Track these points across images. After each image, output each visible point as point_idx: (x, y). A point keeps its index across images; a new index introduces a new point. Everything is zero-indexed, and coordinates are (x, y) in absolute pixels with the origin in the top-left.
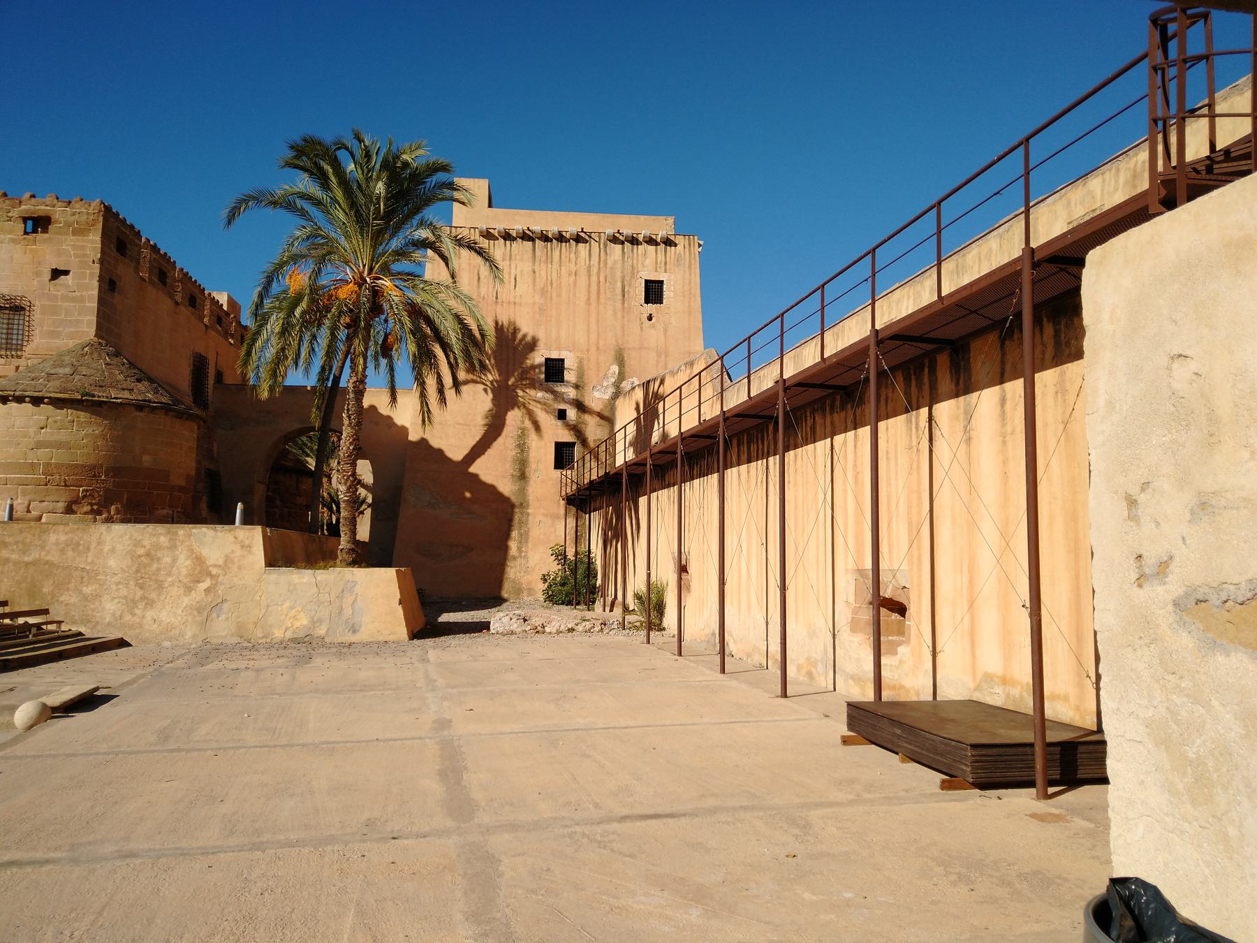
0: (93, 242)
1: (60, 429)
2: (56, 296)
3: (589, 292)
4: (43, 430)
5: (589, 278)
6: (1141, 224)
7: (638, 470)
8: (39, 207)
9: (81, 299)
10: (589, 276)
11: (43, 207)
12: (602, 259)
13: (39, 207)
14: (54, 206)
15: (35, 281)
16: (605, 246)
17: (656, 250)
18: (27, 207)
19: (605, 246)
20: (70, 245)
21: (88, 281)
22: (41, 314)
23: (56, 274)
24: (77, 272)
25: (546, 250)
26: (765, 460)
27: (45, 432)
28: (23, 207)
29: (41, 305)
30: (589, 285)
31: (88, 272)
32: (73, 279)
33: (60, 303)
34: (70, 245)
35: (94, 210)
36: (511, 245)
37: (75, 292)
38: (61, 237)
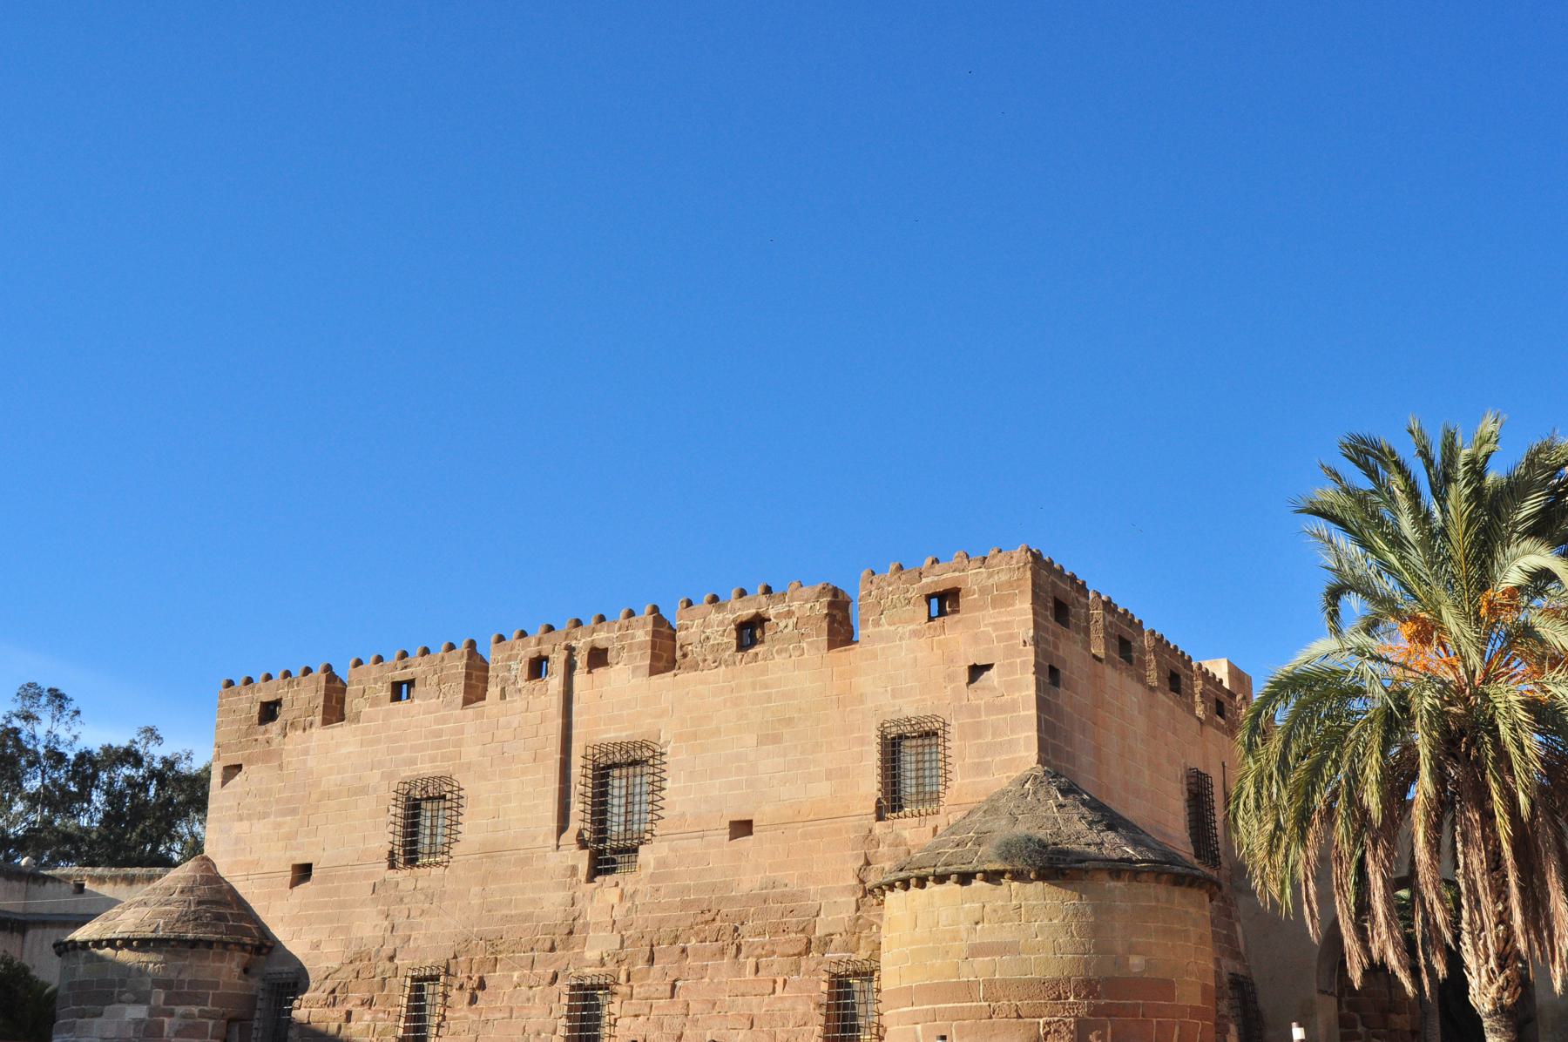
4: (979, 927)
8: (945, 576)
11: (949, 575)
13: (945, 576)
22: (960, 738)
23: (976, 671)
33: (984, 718)
35: (1018, 563)
37: (1003, 695)
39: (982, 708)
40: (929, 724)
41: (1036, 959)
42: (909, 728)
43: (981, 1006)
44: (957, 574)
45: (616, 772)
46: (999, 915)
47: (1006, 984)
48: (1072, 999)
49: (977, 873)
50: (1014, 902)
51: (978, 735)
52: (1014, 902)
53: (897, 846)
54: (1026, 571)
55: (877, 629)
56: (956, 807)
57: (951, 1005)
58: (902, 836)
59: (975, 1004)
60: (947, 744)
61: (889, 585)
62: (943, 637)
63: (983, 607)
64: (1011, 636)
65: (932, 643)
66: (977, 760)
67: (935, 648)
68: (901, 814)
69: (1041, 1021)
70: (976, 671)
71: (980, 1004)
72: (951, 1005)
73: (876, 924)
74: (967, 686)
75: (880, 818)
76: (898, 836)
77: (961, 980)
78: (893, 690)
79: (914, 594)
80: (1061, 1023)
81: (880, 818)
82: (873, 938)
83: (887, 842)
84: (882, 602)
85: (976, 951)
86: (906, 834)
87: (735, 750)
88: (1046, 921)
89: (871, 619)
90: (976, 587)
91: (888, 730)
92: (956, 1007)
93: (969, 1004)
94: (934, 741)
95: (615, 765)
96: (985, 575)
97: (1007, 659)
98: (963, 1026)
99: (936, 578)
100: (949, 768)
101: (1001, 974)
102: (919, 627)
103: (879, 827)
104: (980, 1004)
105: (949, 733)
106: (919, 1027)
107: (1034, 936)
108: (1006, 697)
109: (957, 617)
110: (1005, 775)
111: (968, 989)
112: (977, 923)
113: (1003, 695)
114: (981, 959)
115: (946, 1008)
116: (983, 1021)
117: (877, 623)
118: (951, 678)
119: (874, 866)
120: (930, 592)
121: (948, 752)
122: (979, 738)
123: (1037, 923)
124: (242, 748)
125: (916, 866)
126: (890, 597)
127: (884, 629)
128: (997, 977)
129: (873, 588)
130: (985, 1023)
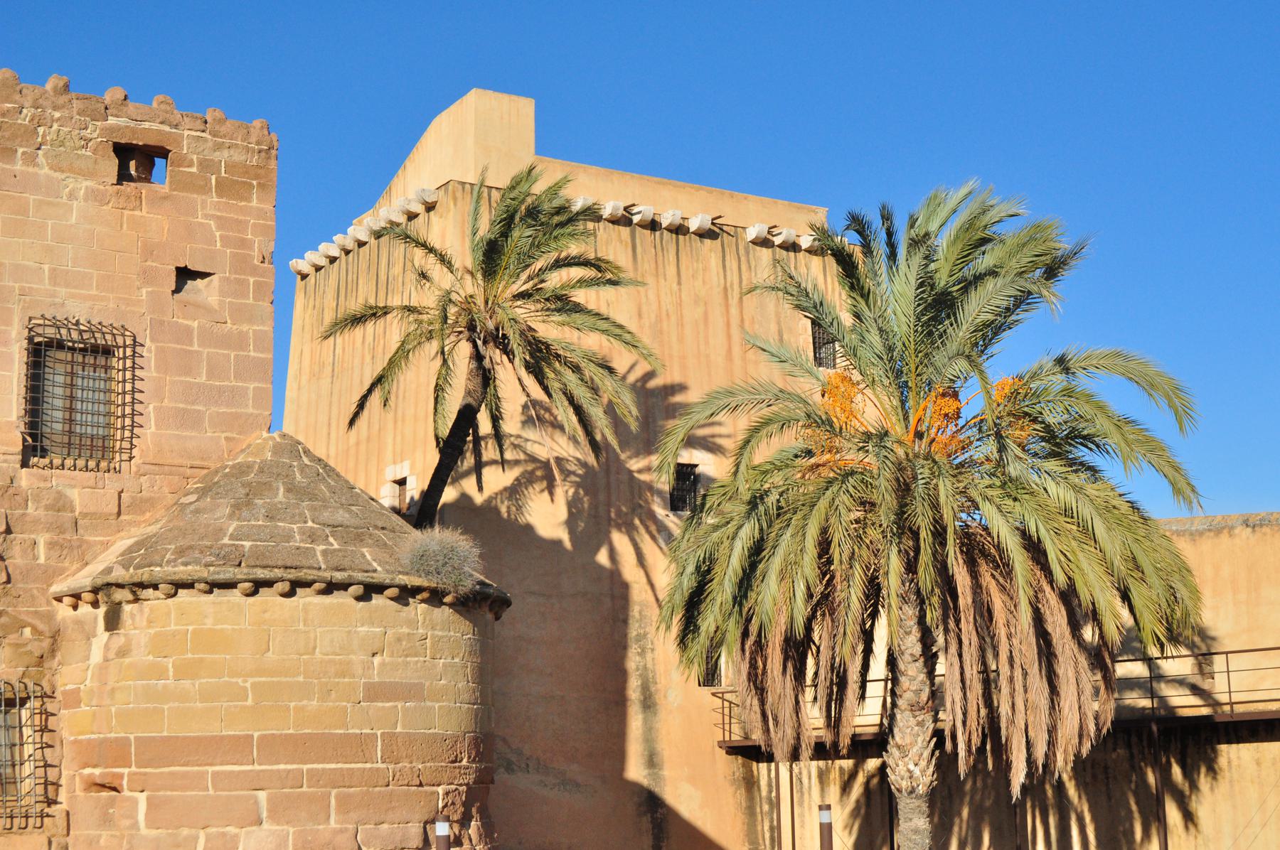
0: (260, 214)
1: (407, 656)
2: (242, 338)
3: (729, 336)
4: (377, 660)
5: (728, 311)
6: (426, 129)
7: (43, 454)
8: (146, 125)
9: (240, 342)
10: (727, 306)
11: (155, 126)
12: (743, 277)
13: (146, 125)
14: (176, 126)
15: (144, 291)
16: (747, 253)
17: (824, 261)
18: (123, 125)
19: (747, 253)
20: (213, 217)
21: (251, 301)
22: (158, 368)
23: (185, 275)
24: (228, 279)
25: (653, 250)
26: (61, 421)
27: (383, 664)
28: (112, 120)
29: (157, 347)
30: (728, 325)
31: (252, 280)
32: (222, 293)
33: (196, 347)
34: (213, 217)
35: (258, 143)
36: (796, 257)
37: (226, 323)
38: (195, 196)
39: (196, 333)
40: (108, 337)
41: (440, 708)
42: (75, 335)
43: (378, 769)
44: (167, 128)
45: (61, 355)
46: (403, 647)
47: (410, 739)
48: (464, 762)
49: (351, 585)
50: (421, 631)
51: (188, 371)
52: (421, 631)
53: (59, 511)
54: (269, 158)
55: (31, 169)
56: (157, 468)
57: (333, 766)
58: (66, 497)
59: (368, 765)
60: (138, 372)
61: (55, 108)
62: (137, 213)
63: (204, 189)
64: (244, 243)
65: (122, 216)
66: (181, 406)
67: (125, 226)
68: (46, 461)
69: (441, 790)
70: (185, 275)
71: (375, 765)
72: (333, 766)
73: (29, 625)
74: (173, 295)
75: (25, 464)
76: (60, 495)
77: (351, 731)
78: (53, 271)
79: (95, 135)
80: (457, 792)
81: (25, 464)
82: (29, 648)
83: (44, 502)
84: (41, 130)
85: (375, 692)
86: (75, 495)
87: (206, 350)
88: (449, 660)
89: (20, 150)
90: (195, 157)
91: (40, 330)
92: (341, 769)
93: (360, 765)
94: (101, 360)
95: (60, 345)
96: (210, 144)
97: (235, 273)
98: (349, 796)
99: (132, 124)
100: (137, 407)
101: (404, 727)
102: (101, 187)
103: (26, 478)
104: (375, 765)
105: (142, 357)
106: (262, 795)
107: (439, 677)
108: (229, 325)
109: (144, 188)
110: (224, 435)
111: (359, 746)
112: (374, 655)
113: (226, 323)
114: (380, 704)
115: (323, 770)
116: (378, 789)
117: (31, 159)
118: (147, 276)
119: (17, 536)
120: (123, 141)
121: (138, 385)
122: (188, 373)
123: (442, 661)
124: (219, 210)
125: (280, 563)
126: (55, 126)
127: (42, 172)
128: (399, 730)
129: (26, 104)
130: (380, 792)
